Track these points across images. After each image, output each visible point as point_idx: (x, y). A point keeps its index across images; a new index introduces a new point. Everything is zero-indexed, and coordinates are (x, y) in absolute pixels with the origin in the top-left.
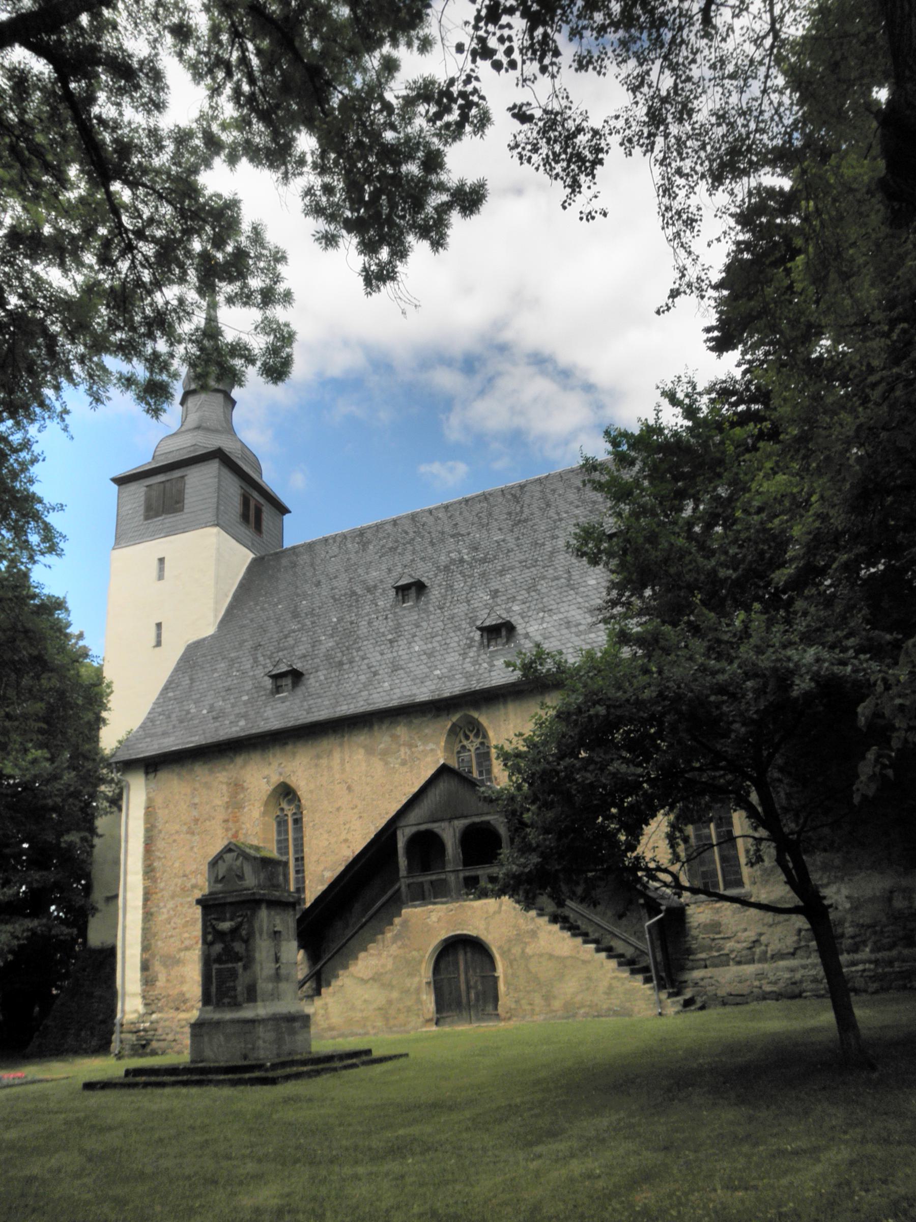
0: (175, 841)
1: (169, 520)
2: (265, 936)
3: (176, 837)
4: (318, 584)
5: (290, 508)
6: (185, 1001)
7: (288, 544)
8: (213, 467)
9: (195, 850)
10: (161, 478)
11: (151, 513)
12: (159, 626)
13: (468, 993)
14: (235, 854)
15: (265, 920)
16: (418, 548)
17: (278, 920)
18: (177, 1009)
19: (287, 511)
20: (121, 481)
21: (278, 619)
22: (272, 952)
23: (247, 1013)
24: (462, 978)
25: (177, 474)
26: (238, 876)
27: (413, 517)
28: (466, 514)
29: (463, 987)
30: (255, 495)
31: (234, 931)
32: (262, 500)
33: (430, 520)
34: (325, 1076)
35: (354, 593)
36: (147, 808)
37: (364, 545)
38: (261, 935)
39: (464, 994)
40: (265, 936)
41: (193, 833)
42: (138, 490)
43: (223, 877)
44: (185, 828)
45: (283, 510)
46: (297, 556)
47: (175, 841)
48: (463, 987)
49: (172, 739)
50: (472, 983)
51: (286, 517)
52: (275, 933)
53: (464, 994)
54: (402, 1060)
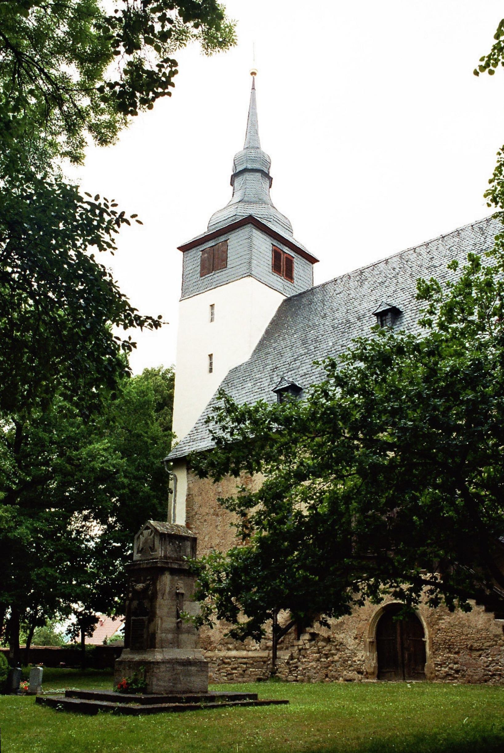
0: (205, 521)
1: (218, 275)
2: (167, 596)
3: (206, 517)
4: (325, 316)
5: (319, 259)
6: (211, 643)
7: (315, 285)
8: (248, 230)
9: (219, 528)
10: (211, 244)
11: (206, 270)
12: (211, 356)
13: (403, 654)
14: (150, 531)
15: (168, 582)
16: (401, 280)
17: (180, 584)
18: (206, 649)
19: (317, 261)
20: (184, 249)
21: (292, 346)
22: (174, 609)
23: (148, 657)
24: (399, 639)
25: (222, 239)
26: (150, 548)
27: (401, 256)
28: (441, 248)
29: (398, 647)
30: (286, 250)
31: (145, 590)
32: (292, 254)
33: (413, 257)
34: (189, 713)
35: (348, 321)
36: (188, 495)
37: (362, 283)
38: (163, 594)
39: (400, 654)
40: (167, 596)
41: (217, 515)
42: (197, 254)
43: (142, 549)
44: (212, 511)
45: (312, 260)
46: (314, 295)
47: (205, 521)
48: (398, 647)
49: (206, 442)
50: (406, 646)
51: (316, 265)
52: (178, 594)
53: (400, 654)
54: (283, 706)
